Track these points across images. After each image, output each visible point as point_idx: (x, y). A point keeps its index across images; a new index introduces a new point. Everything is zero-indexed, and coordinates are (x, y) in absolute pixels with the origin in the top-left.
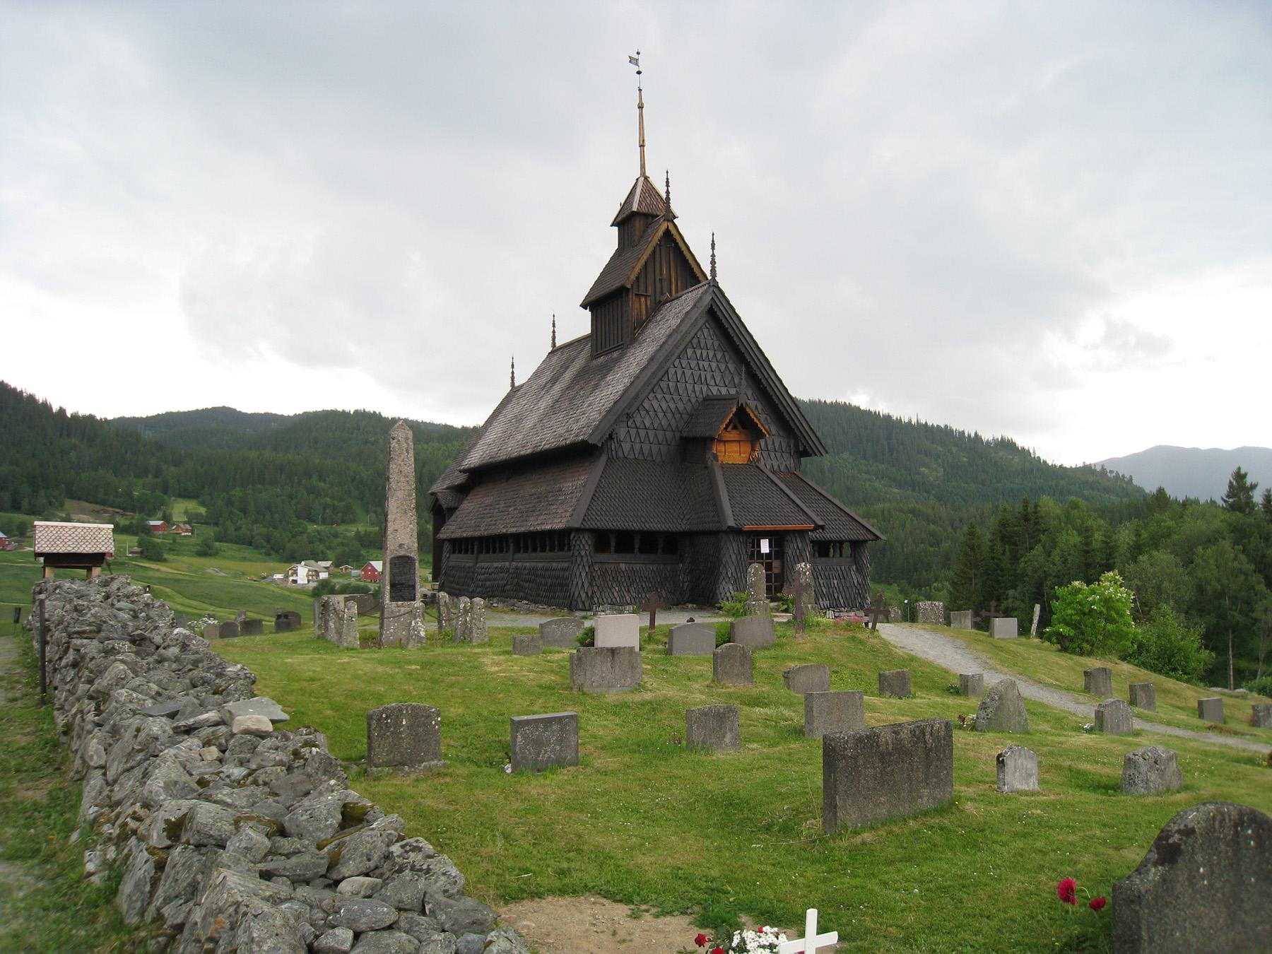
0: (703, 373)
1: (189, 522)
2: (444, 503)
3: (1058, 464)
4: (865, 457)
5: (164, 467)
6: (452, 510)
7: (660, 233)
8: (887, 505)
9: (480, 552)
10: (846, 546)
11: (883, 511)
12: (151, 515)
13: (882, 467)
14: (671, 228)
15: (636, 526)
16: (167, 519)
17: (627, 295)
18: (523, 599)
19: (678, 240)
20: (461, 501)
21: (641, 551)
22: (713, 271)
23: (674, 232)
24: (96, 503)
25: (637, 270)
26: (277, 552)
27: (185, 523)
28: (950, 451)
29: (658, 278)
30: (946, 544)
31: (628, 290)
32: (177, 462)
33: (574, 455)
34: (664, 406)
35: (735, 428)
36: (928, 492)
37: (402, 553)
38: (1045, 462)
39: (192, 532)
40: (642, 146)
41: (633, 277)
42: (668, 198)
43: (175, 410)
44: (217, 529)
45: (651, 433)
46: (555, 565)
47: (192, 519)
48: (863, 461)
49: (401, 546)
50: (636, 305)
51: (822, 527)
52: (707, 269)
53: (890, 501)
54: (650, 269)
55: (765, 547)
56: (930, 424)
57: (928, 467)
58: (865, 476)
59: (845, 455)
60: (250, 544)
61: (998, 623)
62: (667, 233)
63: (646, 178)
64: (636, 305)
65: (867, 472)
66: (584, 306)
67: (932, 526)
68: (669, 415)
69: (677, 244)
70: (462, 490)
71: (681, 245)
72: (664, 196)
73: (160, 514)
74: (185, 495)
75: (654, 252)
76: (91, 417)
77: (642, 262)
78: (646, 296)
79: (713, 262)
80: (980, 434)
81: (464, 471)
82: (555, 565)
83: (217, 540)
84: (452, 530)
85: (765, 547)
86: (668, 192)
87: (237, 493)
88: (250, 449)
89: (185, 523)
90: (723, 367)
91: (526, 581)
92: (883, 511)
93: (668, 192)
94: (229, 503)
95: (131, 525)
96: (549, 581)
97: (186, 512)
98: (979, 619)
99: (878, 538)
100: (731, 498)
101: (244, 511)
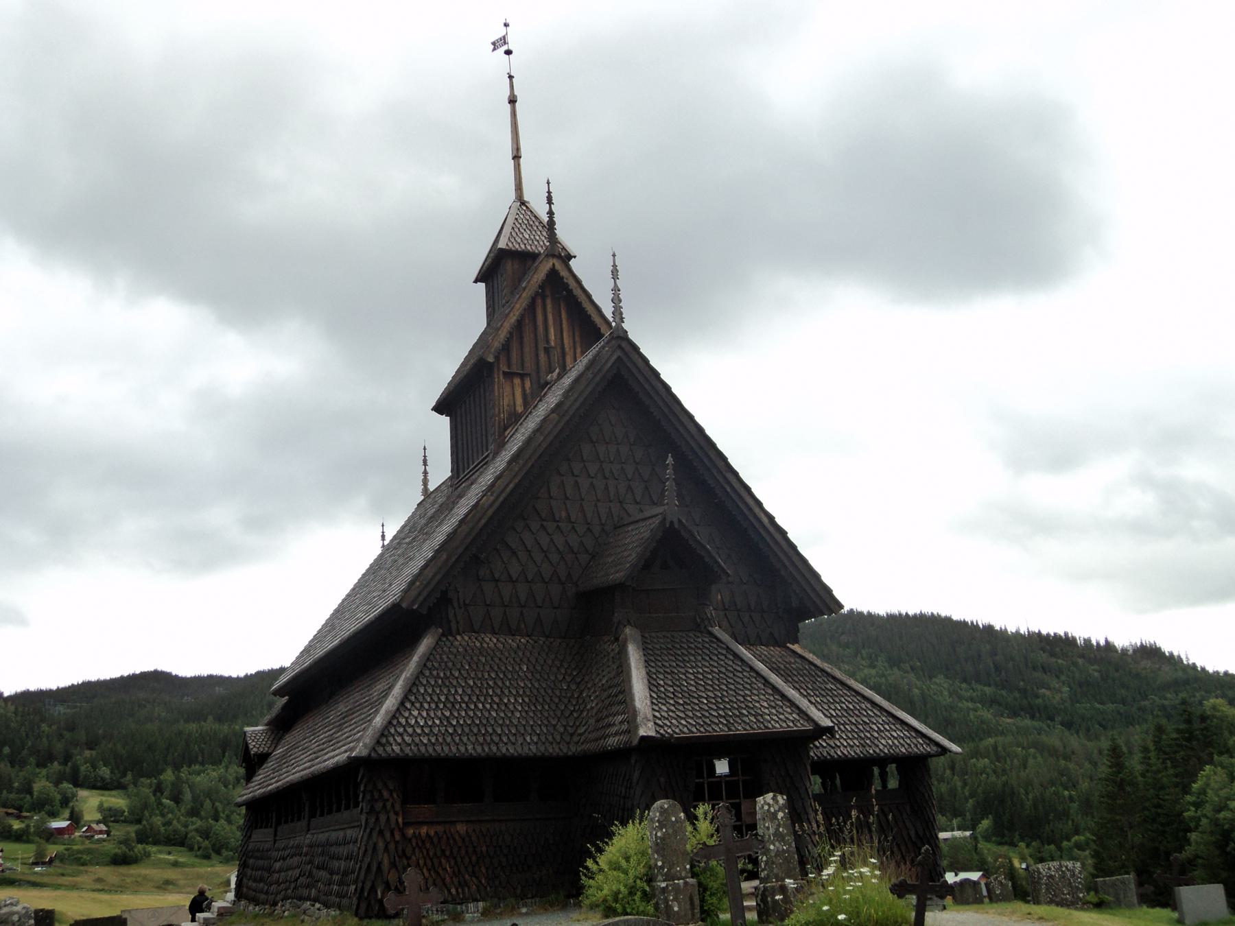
1: (104, 821)
2: (254, 748)
3: (1222, 670)
4: (965, 680)
6: (263, 758)
8: (1000, 738)
10: (892, 768)
11: (995, 748)
12: (54, 815)
16: (75, 819)
18: (315, 900)
19: (572, 284)
22: (618, 312)
23: (564, 273)
26: (218, 852)
27: (98, 822)
28: (1075, 664)
29: (542, 345)
30: (1085, 785)
36: (1052, 719)
38: (1203, 669)
39: (108, 833)
40: (517, 157)
42: (551, 223)
43: (93, 678)
44: (137, 827)
47: (110, 816)
48: (964, 686)
50: (508, 389)
51: (830, 730)
52: (608, 312)
53: (1002, 733)
54: (528, 331)
55: (722, 767)
56: (1044, 632)
57: (1049, 689)
58: (970, 705)
59: (940, 679)
60: (182, 844)
61: (1186, 893)
62: (553, 272)
63: (523, 203)
64: (508, 389)
65: (972, 700)
66: (440, 408)
68: (554, 558)
69: (570, 292)
71: (578, 292)
72: (545, 219)
73: (67, 814)
77: (513, 318)
78: (522, 376)
79: (616, 300)
80: (1110, 639)
81: (280, 692)
83: (140, 841)
84: (268, 781)
85: (722, 767)
86: (551, 213)
87: (168, 776)
88: (187, 721)
91: (318, 868)
92: (995, 748)
93: (551, 213)
94: (158, 789)
97: (101, 808)
98: (1149, 889)
100: (652, 685)
101: (177, 799)
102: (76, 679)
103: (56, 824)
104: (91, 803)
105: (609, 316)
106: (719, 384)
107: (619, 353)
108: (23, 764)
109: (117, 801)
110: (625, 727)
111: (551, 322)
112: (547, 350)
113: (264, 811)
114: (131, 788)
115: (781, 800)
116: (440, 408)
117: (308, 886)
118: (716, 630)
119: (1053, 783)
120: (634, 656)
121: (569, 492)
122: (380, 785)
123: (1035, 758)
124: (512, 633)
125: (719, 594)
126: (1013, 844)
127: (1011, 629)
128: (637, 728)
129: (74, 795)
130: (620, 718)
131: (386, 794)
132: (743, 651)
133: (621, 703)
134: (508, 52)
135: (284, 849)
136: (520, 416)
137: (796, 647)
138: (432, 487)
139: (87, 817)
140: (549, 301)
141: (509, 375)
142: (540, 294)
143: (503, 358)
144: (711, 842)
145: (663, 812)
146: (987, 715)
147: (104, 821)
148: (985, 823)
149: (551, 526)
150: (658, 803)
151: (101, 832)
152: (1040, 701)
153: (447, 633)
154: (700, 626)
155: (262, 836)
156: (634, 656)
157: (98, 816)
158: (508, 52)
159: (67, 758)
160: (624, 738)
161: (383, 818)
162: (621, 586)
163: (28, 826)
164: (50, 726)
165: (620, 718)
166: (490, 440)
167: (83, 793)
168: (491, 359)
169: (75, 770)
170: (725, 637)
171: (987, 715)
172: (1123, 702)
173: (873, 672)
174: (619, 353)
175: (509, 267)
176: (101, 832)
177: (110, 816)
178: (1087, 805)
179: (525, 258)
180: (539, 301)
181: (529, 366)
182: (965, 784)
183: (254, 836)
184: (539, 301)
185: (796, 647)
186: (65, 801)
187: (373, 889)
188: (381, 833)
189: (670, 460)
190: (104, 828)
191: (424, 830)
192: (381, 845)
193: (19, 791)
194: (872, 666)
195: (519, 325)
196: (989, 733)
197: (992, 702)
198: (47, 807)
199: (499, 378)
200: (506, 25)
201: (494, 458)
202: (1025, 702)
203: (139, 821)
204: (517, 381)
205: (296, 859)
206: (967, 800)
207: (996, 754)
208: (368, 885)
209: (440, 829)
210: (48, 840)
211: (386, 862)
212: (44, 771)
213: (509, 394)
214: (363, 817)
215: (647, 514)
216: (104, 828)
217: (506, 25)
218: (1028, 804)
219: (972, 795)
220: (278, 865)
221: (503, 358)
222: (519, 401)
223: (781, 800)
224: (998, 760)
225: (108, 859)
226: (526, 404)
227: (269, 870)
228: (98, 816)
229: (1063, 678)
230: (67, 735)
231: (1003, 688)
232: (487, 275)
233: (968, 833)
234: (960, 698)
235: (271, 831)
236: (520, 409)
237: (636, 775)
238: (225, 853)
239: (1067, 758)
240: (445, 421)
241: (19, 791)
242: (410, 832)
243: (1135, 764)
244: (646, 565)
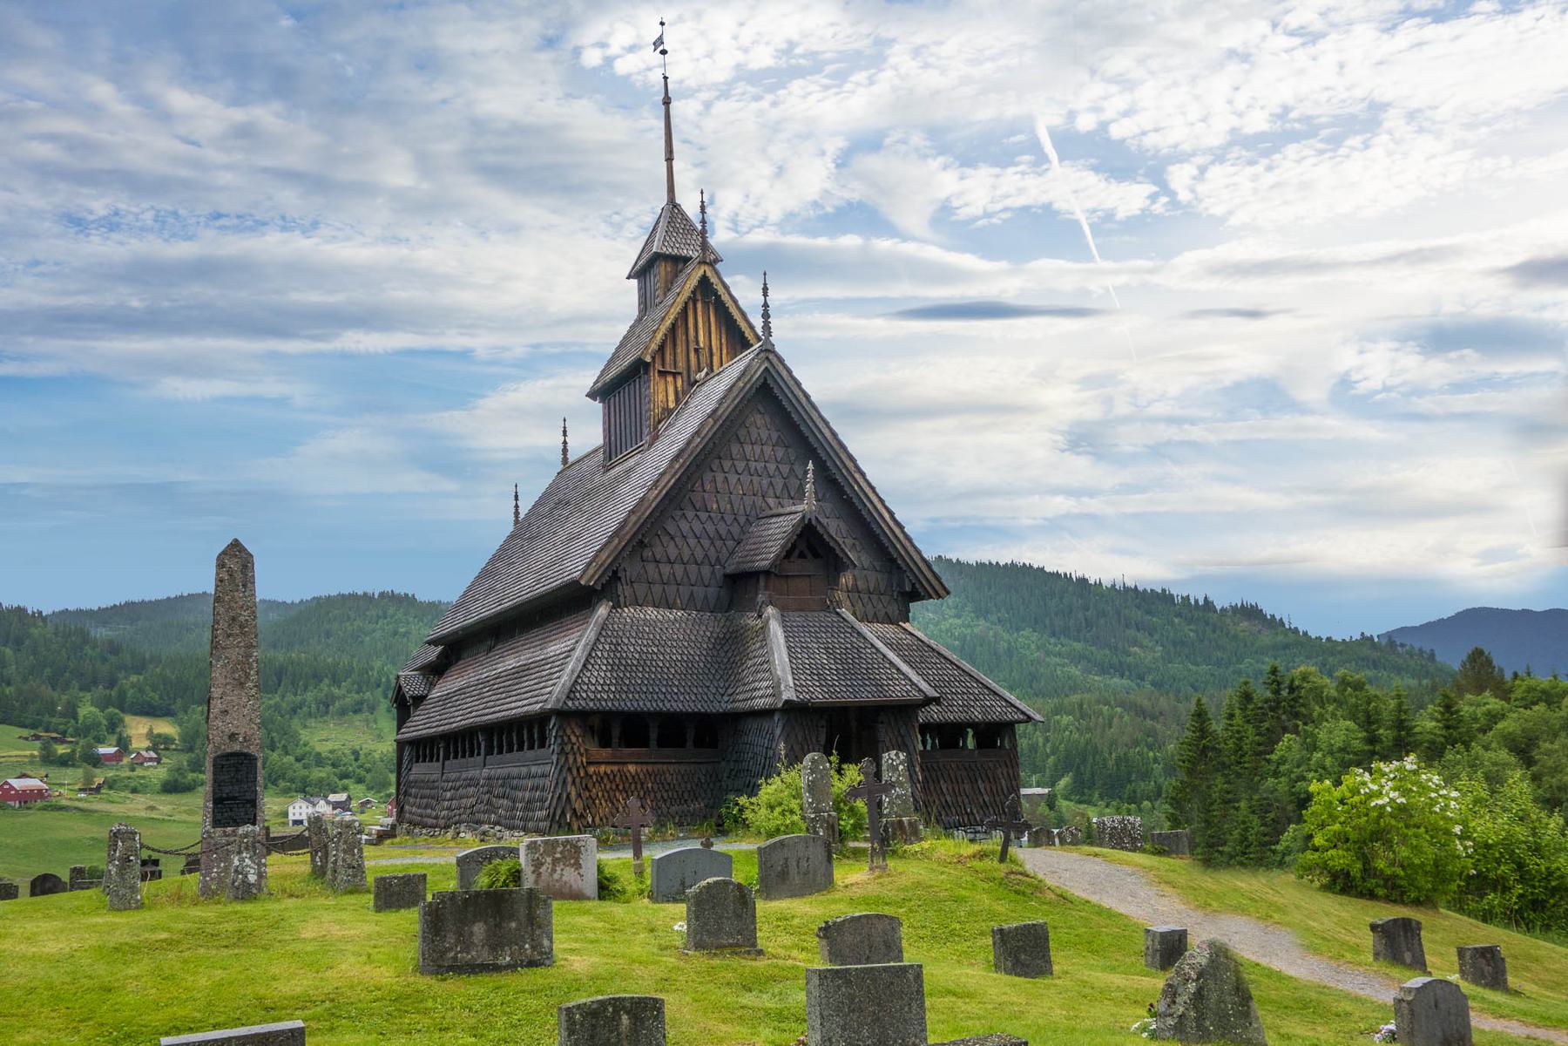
0: (755, 478)
1: (154, 748)
2: (410, 691)
4: (1053, 634)
5: (121, 675)
6: (419, 700)
7: (693, 282)
8: (1087, 696)
9: (489, 752)
11: (1081, 705)
12: (100, 741)
13: (1078, 646)
14: (709, 274)
15: (650, 706)
16: (124, 745)
17: (647, 372)
18: (497, 823)
20: (432, 685)
21: (661, 744)
22: (767, 327)
23: (713, 280)
24: (24, 726)
25: (659, 336)
26: (274, 783)
28: (1172, 623)
29: (692, 346)
31: (647, 365)
32: (139, 668)
33: (567, 603)
34: (697, 527)
35: (802, 556)
36: (1142, 679)
37: (237, 748)
40: (669, 159)
41: (654, 346)
42: (703, 233)
43: (136, 598)
45: (679, 569)
46: (534, 769)
47: (159, 744)
48: (1052, 640)
49: (233, 737)
51: (937, 701)
52: (758, 323)
53: (1089, 690)
54: (680, 332)
57: (1141, 647)
63: (676, 206)
64: (661, 387)
65: (1059, 654)
66: (592, 395)
67: (1149, 722)
68: (706, 543)
69: (718, 297)
70: (435, 670)
74: (150, 711)
75: (685, 311)
76: (20, 611)
77: (668, 323)
78: (674, 375)
81: (434, 642)
82: (534, 769)
84: (422, 724)
86: (703, 222)
89: (148, 749)
90: (785, 469)
91: (498, 797)
93: (703, 222)
95: (72, 755)
96: (527, 794)
99: (1029, 719)
102: (119, 600)
103: (103, 750)
104: (139, 730)
105: (760, 332)
106: (834, 356)
107: (766, 364)
108: (67, 686)
109: (165, 728)
110: (770, 691)
111: (700, 325)
112: (696, 351)
113: (418, 749)
114: (180, 715)
115: (902, 756)
116: (592, 395)
117: (485, 812)
118: (845, 612)
119: (1136, 743)
120: (776, 630)
121: (719, 485)
122: (569, 732)
123: (1121, 717)
124: (670, 607)
125: (846, 579)
126: (1089, 803)
127: (1106, 583)
128: (780, 693)
129: (122, 720)
130: (765, 684)
131: (574, 739)
132: (864, 628)
133: (765, 671)
134: (664, 52)
135: (458, 779)
136: (670, 412)
137: (907, 626)
138: (571, 458)
139: (135, 745)
140: (699, 306)
141: (663, 374)
142: (693, 299)
143: (658, 360)
144: (743, 800)
145: (813, 761)
146: (1075, 671)
147: (154, 748)
148: (1063, 782)
149: (703, 516)
150: (809, 756)
151: (151, 759)
152: (1130, 659)
153: (617, 606)
154: (830, 608)
155: (420, 770)
156: (776, 630)
157: (147, 744)
158: (664, 52)
159: (112, 683)
160: (769, 701)
161: (571, 760)
162: (767, 573)
163: (73, 751)
164: (94, 648)
165: (765, 684)
166: (646, 431)
167: (128, 719)
168: (648, 359)
169: (122, 695)
170: (851, 618)
171: (1075, 671)
172: (1219, 664)
173: (959, 622)
174: (766, 364)
175: (662, 269)
176: (151, 759)
177: (159, 744)
178: (1170, 771)
179: (679, 262)
180: (691, 305)
181: (681, 365)
182: (1047, 740)
183: (414, 770)
184: (691, 305)
185: (907, 626)
186: (114, 725)
187: (563, 814)
188: (570, 769)
189: (810, 466)
190: (154, 755)
191: (602, 768)
192: (569, 779)
193: (63, 715)
194: (958, 616)
195: (673, 327)
196: (1074, 689)
197: (1077, 659)
198: (90, 731)
199: (654, 375)
200: (662, 24)
201: (651, 445)
202: (1115, 660)
203: (191, 750)
204: (670, 379)
205: (472, 790)
206: (1048, 757)
207: (1081, 712)
208: (559, 812)
209: (615, 768)
210: (95, 766)
211: (573, 794)
212: (88, 696)
213: (661, 392)
214: (555, 757)
215: (788, 509)
216: (154, 755)
217: (662, 24)
218: (1110, 763)
219: (1054, 751)
220: (449, 794)
221: (658, 360)
222: (672, 397)
223: (902, 756)
224: (1082, 717)
225: (158, 787)
226: (677, 401)
227: (437, 799)
228: (147, 744)
229: (1156, 637)
230: (113, 658)
231: (1094, 644)
232: (642, 272)
233: (1046, 791)
234: (1048, 653)
235: (437, 765)
236: (672, 405)
237: (778, 732)
238: (282, 784)
239: (1153, 718)
240: (598, 406)
241: (63, 715)
242: (591, 769)
243: (1218, 727)
244: (789, 553)
